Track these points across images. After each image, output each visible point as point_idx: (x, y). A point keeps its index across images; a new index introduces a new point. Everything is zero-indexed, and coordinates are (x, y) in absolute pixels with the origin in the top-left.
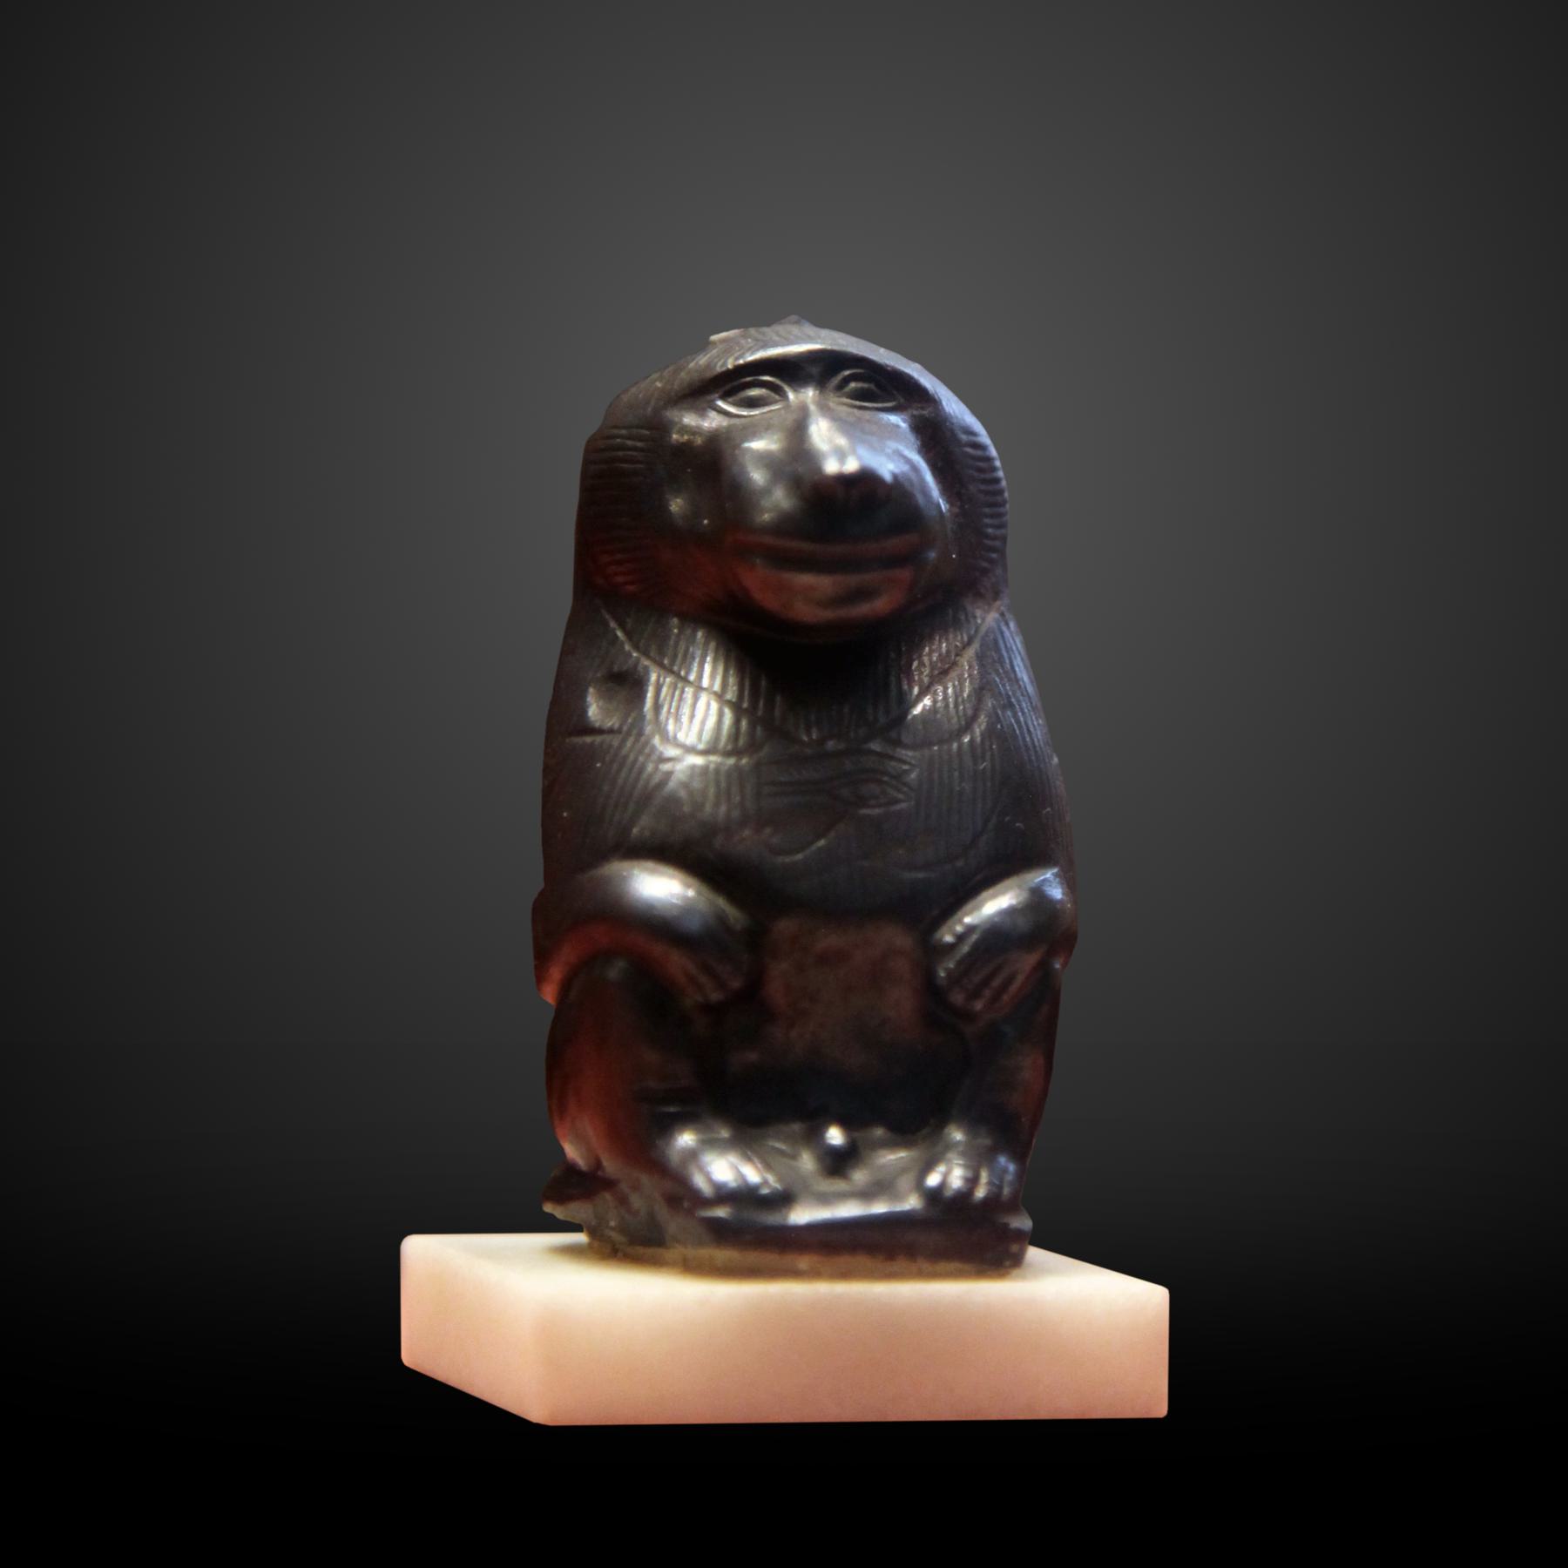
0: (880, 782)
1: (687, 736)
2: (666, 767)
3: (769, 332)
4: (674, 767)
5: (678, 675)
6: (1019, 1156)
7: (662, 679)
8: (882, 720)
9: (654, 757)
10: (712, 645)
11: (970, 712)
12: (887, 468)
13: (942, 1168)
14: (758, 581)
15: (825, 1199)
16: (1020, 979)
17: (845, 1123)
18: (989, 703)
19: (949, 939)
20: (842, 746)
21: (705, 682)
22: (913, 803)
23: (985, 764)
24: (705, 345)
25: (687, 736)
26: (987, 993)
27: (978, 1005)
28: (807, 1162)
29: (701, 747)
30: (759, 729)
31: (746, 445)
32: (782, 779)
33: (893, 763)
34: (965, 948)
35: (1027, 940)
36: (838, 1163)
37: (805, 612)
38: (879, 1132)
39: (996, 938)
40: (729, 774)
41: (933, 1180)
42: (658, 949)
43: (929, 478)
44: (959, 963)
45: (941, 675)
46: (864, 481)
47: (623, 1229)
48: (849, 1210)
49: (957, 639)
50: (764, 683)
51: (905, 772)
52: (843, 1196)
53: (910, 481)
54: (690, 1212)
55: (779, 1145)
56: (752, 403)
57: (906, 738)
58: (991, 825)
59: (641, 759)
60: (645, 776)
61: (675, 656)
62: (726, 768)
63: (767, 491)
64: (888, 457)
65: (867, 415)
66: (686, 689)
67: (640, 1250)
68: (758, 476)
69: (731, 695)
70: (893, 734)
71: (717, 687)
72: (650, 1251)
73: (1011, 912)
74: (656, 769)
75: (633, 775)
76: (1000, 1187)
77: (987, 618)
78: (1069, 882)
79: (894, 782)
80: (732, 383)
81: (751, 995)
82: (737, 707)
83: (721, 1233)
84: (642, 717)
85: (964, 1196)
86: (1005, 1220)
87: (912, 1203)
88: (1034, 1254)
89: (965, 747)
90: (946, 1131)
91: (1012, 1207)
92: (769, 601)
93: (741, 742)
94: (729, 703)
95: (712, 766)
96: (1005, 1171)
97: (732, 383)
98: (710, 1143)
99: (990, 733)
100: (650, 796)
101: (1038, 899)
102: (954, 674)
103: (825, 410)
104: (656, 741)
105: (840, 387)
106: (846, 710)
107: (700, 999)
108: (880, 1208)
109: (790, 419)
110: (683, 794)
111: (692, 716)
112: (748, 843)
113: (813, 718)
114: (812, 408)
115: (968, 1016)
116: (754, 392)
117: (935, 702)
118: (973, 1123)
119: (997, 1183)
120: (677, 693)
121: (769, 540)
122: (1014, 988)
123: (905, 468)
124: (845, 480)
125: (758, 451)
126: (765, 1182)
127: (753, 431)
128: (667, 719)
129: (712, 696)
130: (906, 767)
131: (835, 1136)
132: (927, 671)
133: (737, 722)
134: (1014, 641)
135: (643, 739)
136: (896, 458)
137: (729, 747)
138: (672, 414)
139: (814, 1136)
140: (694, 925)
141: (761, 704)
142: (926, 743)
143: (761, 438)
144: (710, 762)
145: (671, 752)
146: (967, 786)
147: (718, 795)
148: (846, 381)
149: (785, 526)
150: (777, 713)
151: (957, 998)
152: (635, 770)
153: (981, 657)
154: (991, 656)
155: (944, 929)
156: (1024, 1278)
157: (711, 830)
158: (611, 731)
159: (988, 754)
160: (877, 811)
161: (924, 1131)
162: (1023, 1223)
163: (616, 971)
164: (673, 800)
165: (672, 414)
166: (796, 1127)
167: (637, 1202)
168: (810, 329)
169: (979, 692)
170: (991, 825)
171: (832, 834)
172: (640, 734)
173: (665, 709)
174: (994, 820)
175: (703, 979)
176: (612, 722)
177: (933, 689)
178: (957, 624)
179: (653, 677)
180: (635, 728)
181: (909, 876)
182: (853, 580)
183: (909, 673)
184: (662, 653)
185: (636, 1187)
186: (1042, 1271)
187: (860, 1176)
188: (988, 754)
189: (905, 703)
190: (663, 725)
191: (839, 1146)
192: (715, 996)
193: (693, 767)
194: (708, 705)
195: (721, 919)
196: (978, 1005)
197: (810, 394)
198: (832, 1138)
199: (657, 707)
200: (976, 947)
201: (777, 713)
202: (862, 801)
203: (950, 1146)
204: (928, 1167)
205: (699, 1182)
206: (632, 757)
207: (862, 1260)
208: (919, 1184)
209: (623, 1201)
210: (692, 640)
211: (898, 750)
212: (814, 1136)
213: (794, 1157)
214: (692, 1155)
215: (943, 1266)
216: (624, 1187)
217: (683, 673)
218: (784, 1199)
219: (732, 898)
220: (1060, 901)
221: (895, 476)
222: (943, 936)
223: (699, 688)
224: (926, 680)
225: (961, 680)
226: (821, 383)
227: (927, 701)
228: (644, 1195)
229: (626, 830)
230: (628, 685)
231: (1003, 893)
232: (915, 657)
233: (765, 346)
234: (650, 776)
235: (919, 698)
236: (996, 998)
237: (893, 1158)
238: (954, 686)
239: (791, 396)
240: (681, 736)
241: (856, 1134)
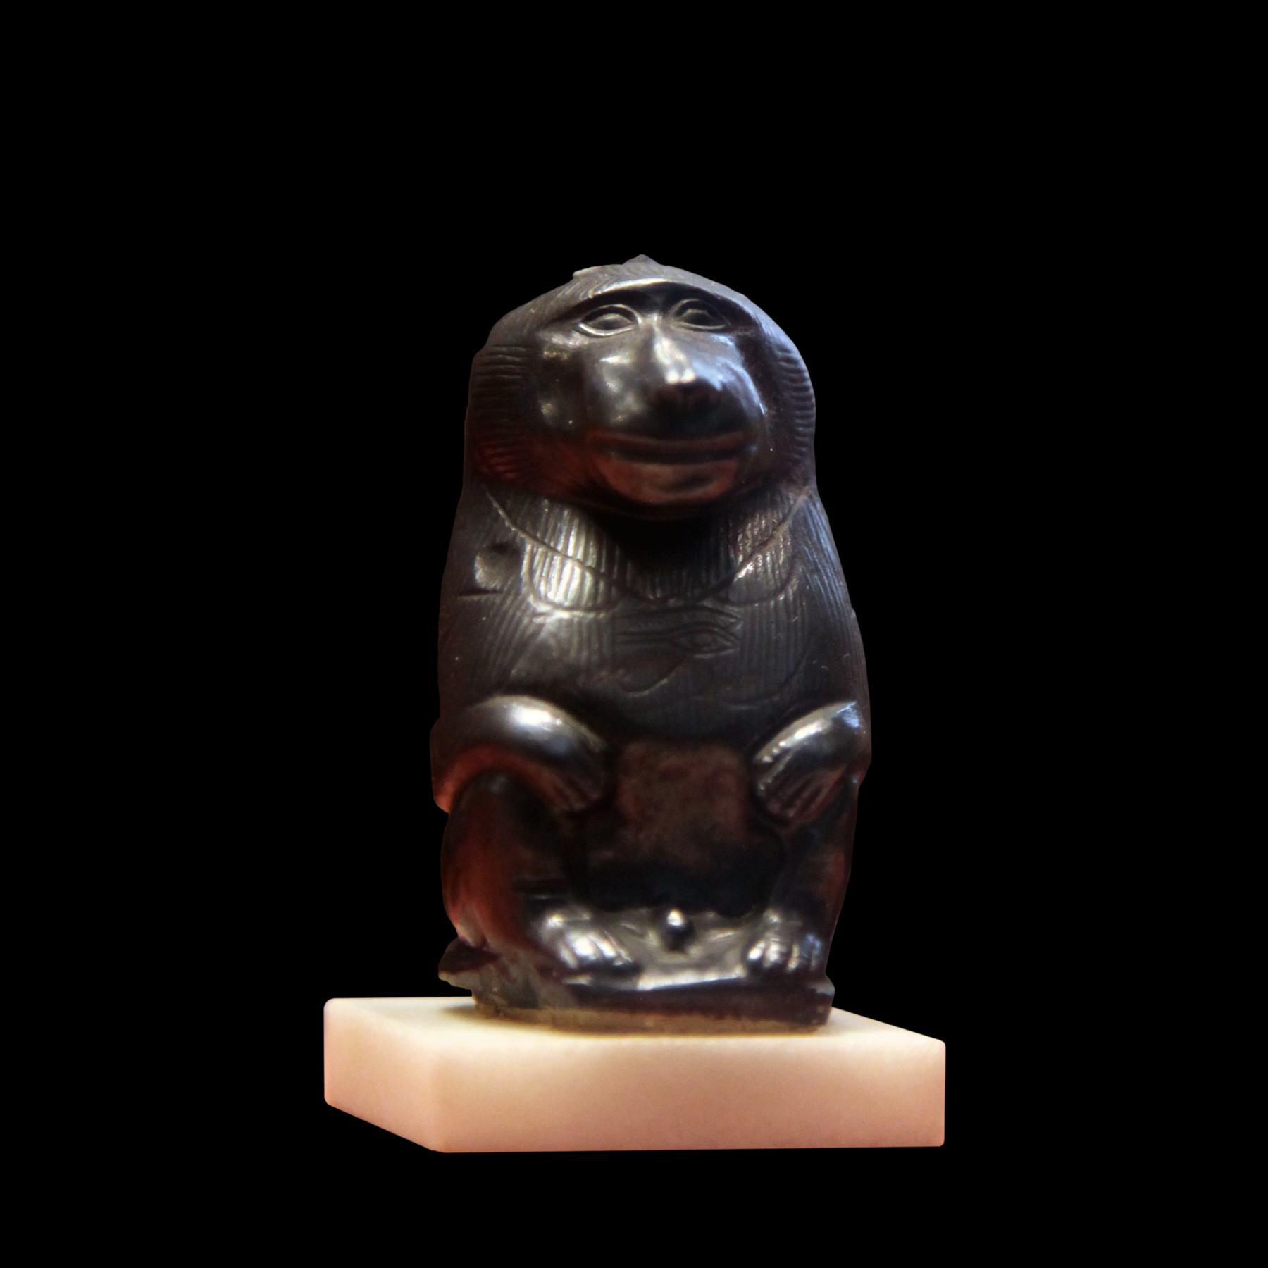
0: (712, 632)
1: (556, 595)
2: (539, 620)
4: (545, 620)
5: (548, 546)
7: (535, 549)
8: (714, 582)
9: (529, 612)
10: (576, 521)
11: (784, 576)
12: (717, 379)
13: (761, 945)
14: (613, 470)
15: (667, 970)
16: (825, 792)
17: (683, 908)
18: (800, 568)
19: (767, 759)
20: (681, 603)
21: (570, 552)
22: (738, 649)
23: (796, 618)
24: (567, 278)
25: (556, 595)
26: (798, 803)
27: (791, 813)
28: (653, 939)
29: (567, 604)
30: (614, 589)
31: (604, 360)
32: (633, 630)
33: (722, 617)
34: (781, 767)
35: (831, 761)
36: (678, 940)
37: (651, 495)
38: (711, 915)
39: (805, 758)
40: (589, 626)
41: (754, 954)
42: (532, 768)
43: (751, 386)
44: (776, 779)
45: (761, 545)
46: (699, 389)
47: (504, 994)
48: (686, 978)
49: (774, 517)
50: (617, 552)
51: (732, 624)
52: (682, 968)
53: (736, 389)
54: (558, 980)
55: (630, 926)
56: (608, 326)
57: (733, 597)
58: (801, 668)
59: (518, 614)
60: (521, 627)
61: (546, 531)
62: (587, 621)
63: (620, 397)
64: (718, 369)
65: (701, 335)
66: (555, 557)
67: (518, 1011)
68: (613, 385)
69: (591, 562)
70: (722, 594)
71: (580, 556)
72: (526, 1012)
73: (817, 737)
74: (531, 622)
75: (512, 627)
76: (809, 960)
79: (723, 633)
80: (592, 310)
81: (608, 805)
82: (596, 572)
83: (583, 997)
84: (519, 580)
85: (779, 967)
86: (813, 987)
87: (737, 973)
88: (836, 1014)
89: (781, 604)
90: (765, 914)
91: (817, 977)
92: (621, 486)
93: (599, 600)
95: (576, 620)
96: (813, 947)
97: (592, 310)
98: (574, 925)
99: (801, 592)
100: (526, 644)
101: (839, 727)
102: (771, 545)
103: (667, 331)
104: (531, 599)
105: (679, 313)
106: (684, 574)
107: (566, 807)
108: (711, 977)
109: (639, 338)
110: (552, 642)
111: (560, 579)
112: (605, 682)
113: (657, 580)
114: (657, 330)
115: (783, 822)
116: (610, 317)
117: (756, 567)
118: (787, 908)
119: (806, 956)
120: (548, 560)
121: (621, 437)
122: (820, 799)
123: (732, 378)
124: (683, 388)
125: (613, 364)
126: (619, 956)
127: (609, 348)
128: (540, 581)
129: (576, 563)
130: (732, 620)
131: (675, 919)
132: (749, 543)
133: (596, 584)
135: (520, 597)
136: (724, 370)
137: (590, 604)
138: (543, 335)
139: (658, 918)
140: (561, 748)
141: (616, 569)
142: (749, 601)
143: (615, 354)
144: (574, 616)
145: (543, 608)
146: (782, 636)
147: (580, 643)
148: (685, 308)
149: (635, 425)
150: (629, 577)
151: (774, 807)
152: (514, 623)
153: (793, 532)
154: (801, 531)
155: (764, 751)
156: (828, 1033)
157: (575, 671)
158: (494, 591)
159: (799, 610)
160: (709, 656)
161: (748, 915)
163: (498, 785)
164: (544, 647)
165: (543, 335)
166: (644, 911)
167: (515, 972)
169: (792, 560)
170: (801, 668)
171: (673, 674)
172: (518, 593)
173: (538, 573)
174: (804, 663)
175: (569, 792)
176: (495, 584)
177: (754, 557)
178: (774, 505)
179: (528, 548)
180: (513, 589)
181: (735, 708)
182: (690, 469)
183: (735, 544)
184: (535, 528)
185: (514, 960)
186: (843, 1028)
187: (695, 951)
188: (799, 610)
189: (732, 569)
190: (536, 586)
191: (679, 926)
192: (578, 806)
193: (561, 620)
194: (573, 570)
195: (583, 743)
196: (791, 813)
197: (655, 318)
198: (673, 920)
199: (531, 572)
200: (789, 766)
201: (629, 577)
202: (697, 648)
203: (768, 927)
204: (750, 944)
205: (566, 955)
206: (511, 612)
207: (697, 1019)
208: (744, 958)
209: (504, 971)
210: (560, 517)
211: (726, 606)
212: (658, 918)
213: (642, 936)
214: (560, 934)
215: (763, 1024)
216: (504, 960)
217: (552, 544)
218: (634, 970)
219: (592, 726)
220: (858, 729)
221: (724, 385)
222: (762, 757)
223: (565, 557)
224: (749, 550)
225: (777, 550)
226: (664, 310)
227: (750, 567)
228: (521, 967)
229: (506, 671)
230: (507, 554)
231: (811, 722)
232: (740, 531)
233: (619, 280)
235: (743, 564)
236: (805, 807)
237: (722, 936)
238: (771, 555)
239: (640, 320)
240: (551, 596)
241: (692, 917)
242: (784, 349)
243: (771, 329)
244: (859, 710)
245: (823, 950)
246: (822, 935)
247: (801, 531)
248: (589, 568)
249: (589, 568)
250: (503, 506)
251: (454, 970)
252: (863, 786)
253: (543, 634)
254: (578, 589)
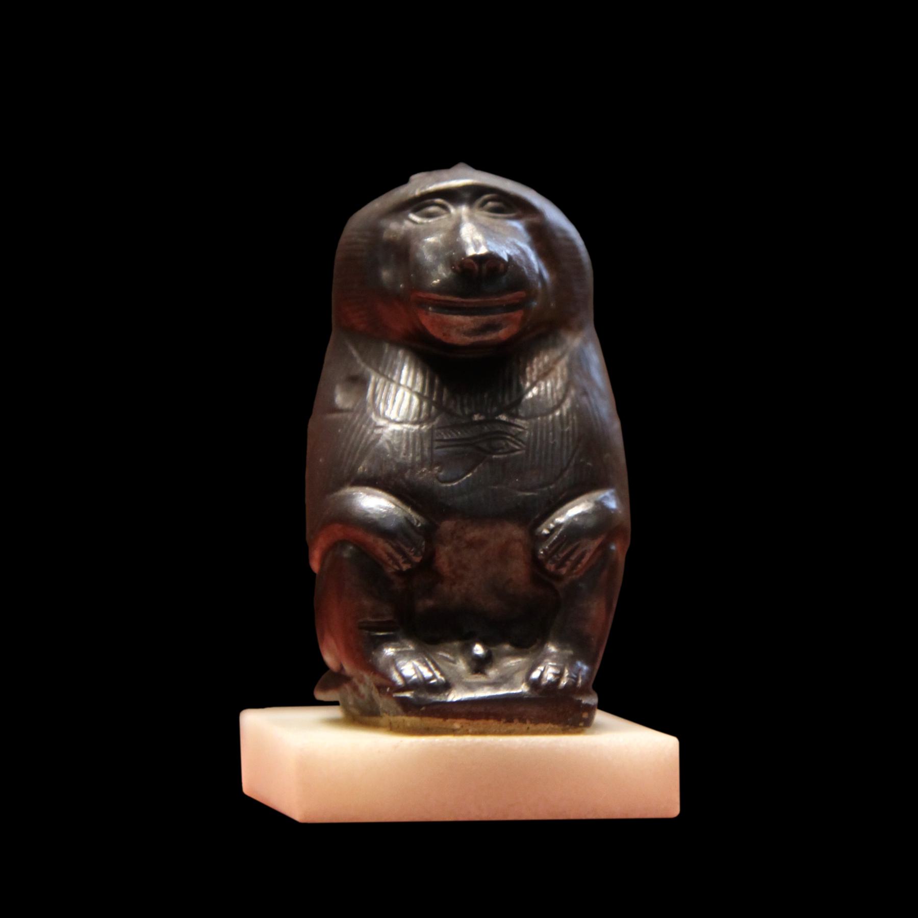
0: (505, 439)
1: (390, 413)
2: (378, 431)
4: (382, 431)
5: (386, 377)
7: (377, 379)
8: (507, 402)
9: (372, 426)
10: (407, 359)
11: (560, 397)
12: (504, 253)
13: (541, 668)
14: (429, 320)
15: (470, 687)
16: (588, 556)
17: (484, 643)
18: (573, 392)
19: (546, 532)
20: (482, 418)
21: (402, 382)
22: (524, 452)
23: (568, 428)
24: (405, 181)
25: (390, 413)
26: (568, 563)
27: (564, 571)
28: (462, 665)
29: (410, 419)
30: (433, 408)
31: (425, 240)
32: (445, 438)
33: (514, 428)
34: (555, 537)
35: (592, 533)
36: (480, 666)
37: (457, 339)
38: (507, 647)
39: (573, 532)
40: (414, 434)
41: (535, 675)
42: (370, 539)
43: (532, 257)
44: (551, 546)
45: (544, 376)
46: (490, 259)
47: (357, 705)
48: (485, 693)
49: (558, 353)
50: (437, 381)
51: (520, 433)
52: (481, 685)
53: (521, 260)
54: (390, 694)
55: (445, 655)
56: (430, 216)
57: (522, 413)
58: (572, 464)
59: (364, 426)
60: (365, 437)
61: (385, 367)
62: (413, 431)
63: (434, 268)
64: (507, 246)
65: (497, 222)
66: (391, 385)
67: (367, 719)
68: (429, 258)
69: (418, 389)
70: (514, 411)
71: (409, 384)
72: (374, 719)
73: (582, 515)
74: (372, 432)
75: (359, 436)
76: (577, 679)
79: (513, 439)
80: (419, 204)
81: (428, 563)
82: (420, 396)
83: (407, 707)
84: (365, 403)
85: (554, 684)
86: (580, 699)
87: (523, 689)
88: (601, 717)
89: (557, 419)
90: (545, 646)
91: (584, 691)
92: (436, 333)
93: (422, 416)
95: (405, 430)
96: (580, 670)
97: (419, 204)
98: (403, 654)
99: (573, 409)
100: (370, 448)
101: (600, 505)
102: (552, 374)
103: (471, 218)
104: (373, 416)
105: (482, 205)
106: (486, 396)
107: (396, 567)
108: (502, 692)
109: (450, 224)
110: (387, 447)
111: (394, 401)
112: (424, 475)
113: (465, 401)
114: (465, 218)
115: (559, 578)
116: (432, 209)
117: (539, 391)
118: (562, 641)
119: (575, 676)
120: (386, 387)
121: (436, 296)
122: (584, 561)
123: (518, 252)
124: (478, 259)
125: (430, 242)
126: (434, 677)
127: (429, 233)
128: (379, 403)
129: (407, 390)
130: (520, 430)
131: (479, 650)
132: (535, 373)
133: (421, 404)
135: (365, 415)
136: (512, 246)
137: (415, 419)
138: (383, 223)
139: (467, 649)
140: (392, 525)
141: (435, 394)
142: (533, 416)
143: (431, 236)
144: (404, 428)
145: (381, 422)
146: (557, 441)
147: (407, 447)
148: (486, 201)
149: (444, 288)
150: (444, 398)
151: (550, 567)
152: (361, 432)
153: (569, 366)
154: (577, 365)
155: (544, 525)
156: (592, 733)
157: (402, 468)
158: (348, 411)
159: (571, 422)
160: (501, 457)
161: (534, 647)
163: (347, 553)
164: (381, 450)
165: (383, 223)
166: (456, 644)
167: (363, 690)
169: (567, 386)
170: (572, 464)
171: (475, 471)
172: (364, 411)
173: (378, 398)
174: (573, 461)
175: (398, 557)
176: (349, 405)
177: (538, 383)
178: (555, 345)
179: (373, 378)
180: (361, 410)
181: (520, 494)
182: (483, 319)
183: (523, 373)
184: (378, 364)
185: (361, 680)
186: (601, 728)
187: (492, 673)
188: (571, 422)
189: (521, 392)
190: (377, 406)
191: (481, 655)
192: (405, 567)
193: (394, 431)
194: (404, 395)
195: (408, 520)
196: (564, 571)
197: (464, 209)
198: (477, 650)
199: (374, 396)
200: (561, 536)
201: (444, 398)
202: (494, 451)
203: (549, 655)
204: (533, 669)
205: (396, 677)
206: (359, 425)
207: (492, 723)
208: (527, 680)
209: (355, 689)
210: (396, 357)
211: (516, 419)
212: (467, 649)
213: (454, 662)
214: (393, 660)
215: (541, 726)
216: (355, 680)
217: (389, 376)
218: (446, 687)
219: (415, 508)
220: (615, 510)
221: (510, 257)
222: (542, 531)
223: (399, 385)
224: (534, 379)
225: (556, 379)
226: (471, 202)
227: (535, 391)
228: (367, 684)
229: (353, 469)
230: (358, 382)
231: (578, 504)
232: (528, 364)
233: (438, 181)
235: (530, 389)
236: (573, 567)
237: (512, 662)
238: (552, 383)
239: (453, 210)
240: (387, 413)
241: (493, 649)
242: (563, 231)
243: (554, 215)
244: (619, 497)
245: (590, 673)
246: (590, 662)
247: (577, 365)
248: (426, 398)
249: (426, 398)
251: (325, 688)
252: (631, 556)
254: (418, 406)
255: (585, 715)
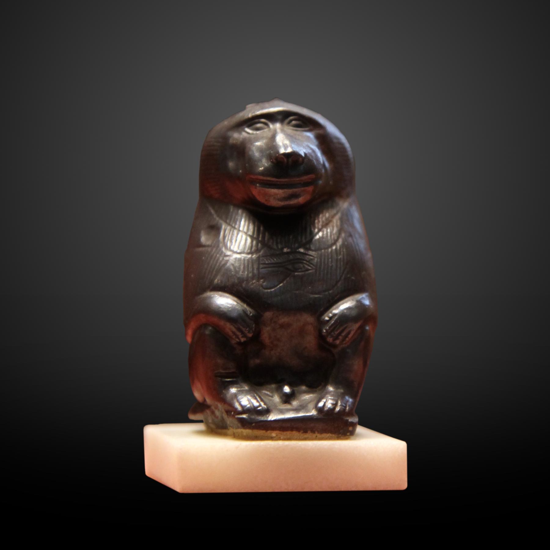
0: (302, 263)
1: (234, 247)
2: (227, 258)
3: (267, 104)
4: (229, 258)
5: (232, 226)
6: (354, 396)
7: (226, 227)
8: (304, 241)
9: (223, 255)
10: (244, 215)
11: (336, 238)
12: (302, 151)
13: (324, 400)
14: (257, 192)
15: (282, 412)
16: (352, 333)
17: (290, 385)
18: (343, 235)
19: (327, 318)
20: (289, 250)
21: (241, 229)
22: (314, 271)
23: (340, 256)
24: (244, 109)
25: (234, 247)
26: (340, 337)
27: (338, 342)
28: (277, 399)
29: (246, 251)
30: (260, 245)
31: (255, 144)
32: (267, 262)
33: (308, 256)
34: (333, 322)
35: (355, 319)
36: (287, 399)
37: (274, 203)
38: (304, 388)
39: (344, 318)
40: (248, 260)
41: (321, 404)
42: (222, 323)
43: (319, 154)
44: (330, 327)
45: (326, 225)
46: (293, 155)
47: (214, 423)
48: (291, 415)
49: (334, 211)
50: (262, 228)
51: (311, 259)
52: (288, 410)
53: (312, 156)
54: (233, 416)
55: (267, 392)
56: (258, 129)
57: (313, 247)
58: (343, 278)
59: (218, 255)
60: (219, 262)
61: (231, 220)
62: (248, 258)
63: (260, 160)
64: (304, 147)
65: (298, 133)
66: (234, 231)
67: (220, 431)
68: (257, 154)
69: (250, 233)
70: (308, 246)
71: (245, 230)
72: (224, 431)
73: (349, 309)
74: (223, 259)
75: (215, 261)
76: (346, 407)
77: (344, 205)
78: (373, 298)
79: (308, 263)
80: (251, 122)
82: (252, 237)
83: (244, 423)
84: (219, 241)
85: (332, 410)
86: (348, 419)
87: (313, 413)
88: (360, 429)
89: (334, 251)
90: (327, 387)
91: (350, 414)
92: (261, 199)
93: (253, 249)
94: (255, 238)
95: (243, 258)
96: (348, 401)
97: (251, 122)
98: (241, 392)
99: (343, 245)
100: (221, 268)
101: (359, 303)
102: (331, 224)
103: (282, 131)
104: (224, 249)
105: (289, 123)
106: (291, 237)
107: (237, 340)
108: (301, 414)
109: (269, 134)
110: (232, 268)
111: (236, 240)
112: (254, 285)
113: (279, 240)
114: (278, 131)
115: (335, 346)
116: (259, 125)
117: (323, 235)
118: (337, 384)
119: (344, 405)
120: (231, 232)
121: (261, 177)
122: (350, 336)
123: (310, 151)
124: (287, 155)
125: (258, 145)
126: (260, 405)
127: (257, 140)
128: (227, 242)
129: (244, 233)
130: (312, 258)
131: (287, 389)
132: (321, 223)
133: (252, 242)
134: (356, 215)
135: (219, 248)
136: (307, 148)
137: (249, 251)
138: (230, 133)
139: (280, 389)
140: (235, 314)
141: (261, 236)
142: (319, 249)
143: (258, 142)
144: (242, 256)
145: (229, 253)
146: (334, 264)
147: (244, 268)
148: (291, 121)
149: (266, 172)
150: (266, 239)
151: (330, 339)
152: (216, 259)
153: (341, 219)
154: (346, 219)
155: (326, 315)
156: (355, 439)
157: (241, 280)
158: (208, 246)
159: (342, 253)
160: (300, 274)
161: (320, 387)
162: (355, 419)
163: (208, 331)
164: (229, 270)
165: (230, 133)
166: (273, 386)
167: (217, 413)
168: (281, 103)
169: (340, 231)
170: (343, 278)
171: (285, 282)
172: (218, 246)
173: (227, 238)
174: (344, 276)
175: (239, 333)
176: (209, 243)
177: (322, 230)
178: (332, 207)
179: (223, 227)
180: (217, 245)
181: (312, 296)
182: (289, 191)
183: (314, 224)
184: (227, 218)
185: (217, 408)
186: (360, 436)
187: (295, 403)
188: (342, 253)
189: (312, 235)
190: (226, 243)
191: (288, 392)
192: (243, 340)
193: (236, 258)
194: (242, 236)
195: (244, 312)
196: (338, 342)
197: (278, 125)
198: (286, 390)
199: (224, 237)
200: (336, 321)
201: (266, 239)
202: (296, 270)
203: (329, 392)
204: (319, 401)
205: (237, 405)
206: (215, 255)
207: (295, 433)
208: (316, 407)
209: (213, 413)
210: (237, 214)
211: (309, 251)
212: (280, 389)
213: (272, 397)
214: (235, 396)
215: (324, 435)
216: (213, 408)
217: (233, 225)
218: (267, 411)
219: (249, 305)
220: (368, 306)
221: (305, 154)
222: (325, 318)
223: (239, 230)
224: (320, 227)
225: (333, 227)
226: (282, 121)
227: (320, 234)
228: (220, 410)
229: (212, 281)
230: (215, 229)
231: (346, 302)
232: (316, 218)
233: (263, 109)
234: (221, 261)
235: (318, 233)
236: (344, 340)
237: (307, 397)
238: (330, 230)
239: (271, 126)
240: (232, 248)
241: (295, 389)
250: (213, 208)
253: (228, 264)
254: (250, 243)
255: (351, 429)
